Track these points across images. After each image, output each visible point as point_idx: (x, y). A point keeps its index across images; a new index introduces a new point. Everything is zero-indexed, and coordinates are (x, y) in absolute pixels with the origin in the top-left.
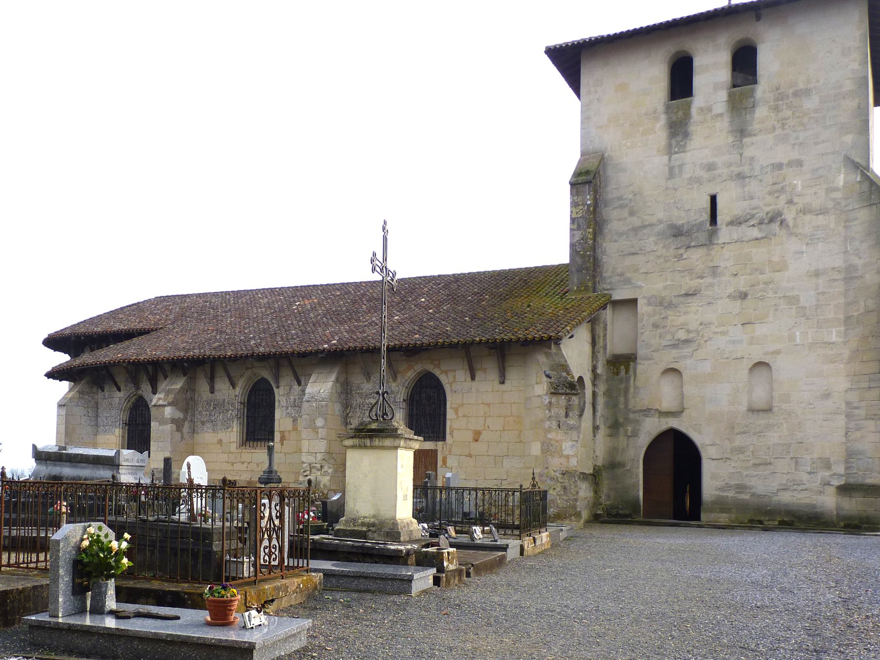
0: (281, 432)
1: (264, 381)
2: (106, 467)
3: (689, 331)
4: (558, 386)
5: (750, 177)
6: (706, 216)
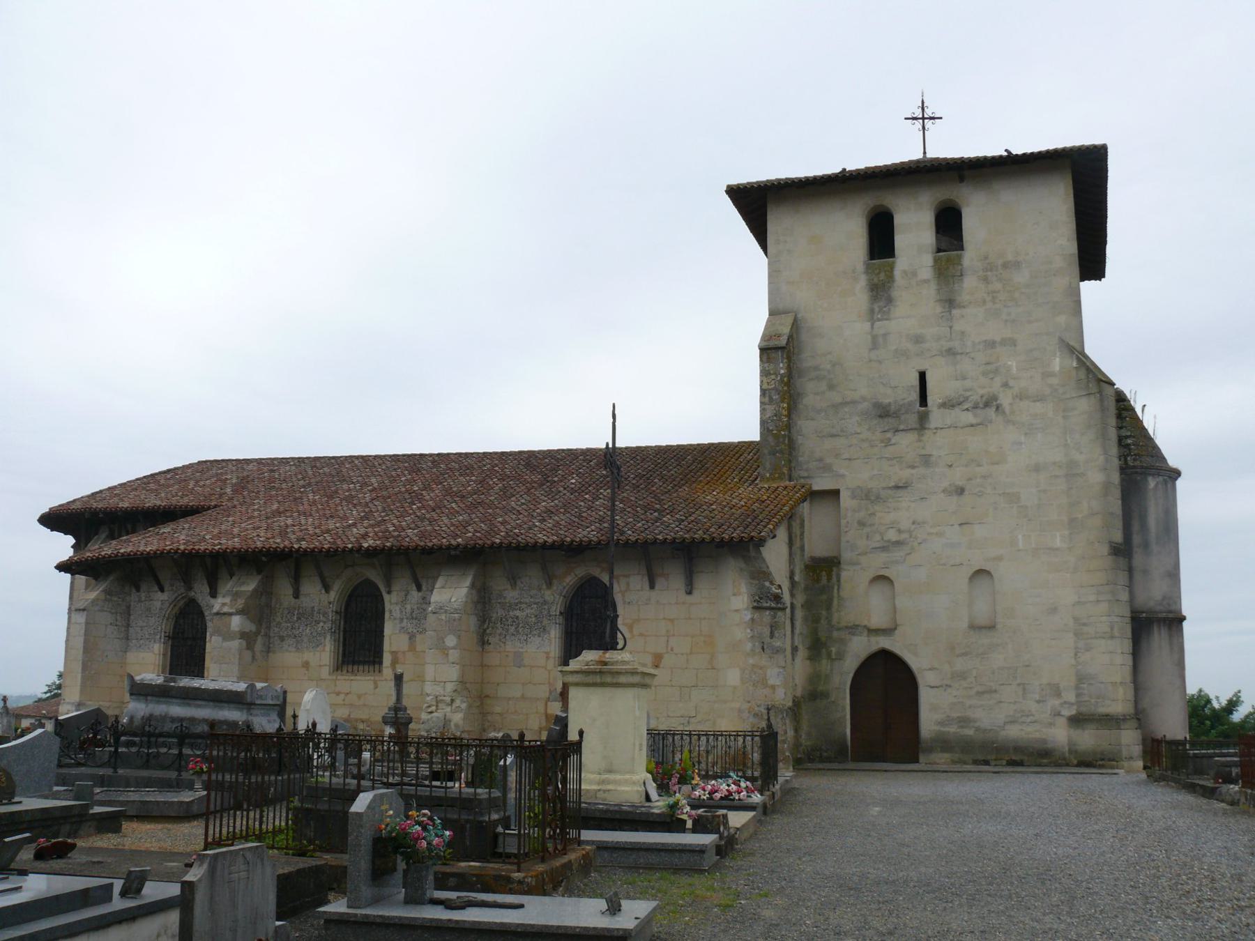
1: (369, 583)
2: (232, 706)
3: (900, 531)
4: (761, 598)
5: (962, 354)
6: (915, 396)
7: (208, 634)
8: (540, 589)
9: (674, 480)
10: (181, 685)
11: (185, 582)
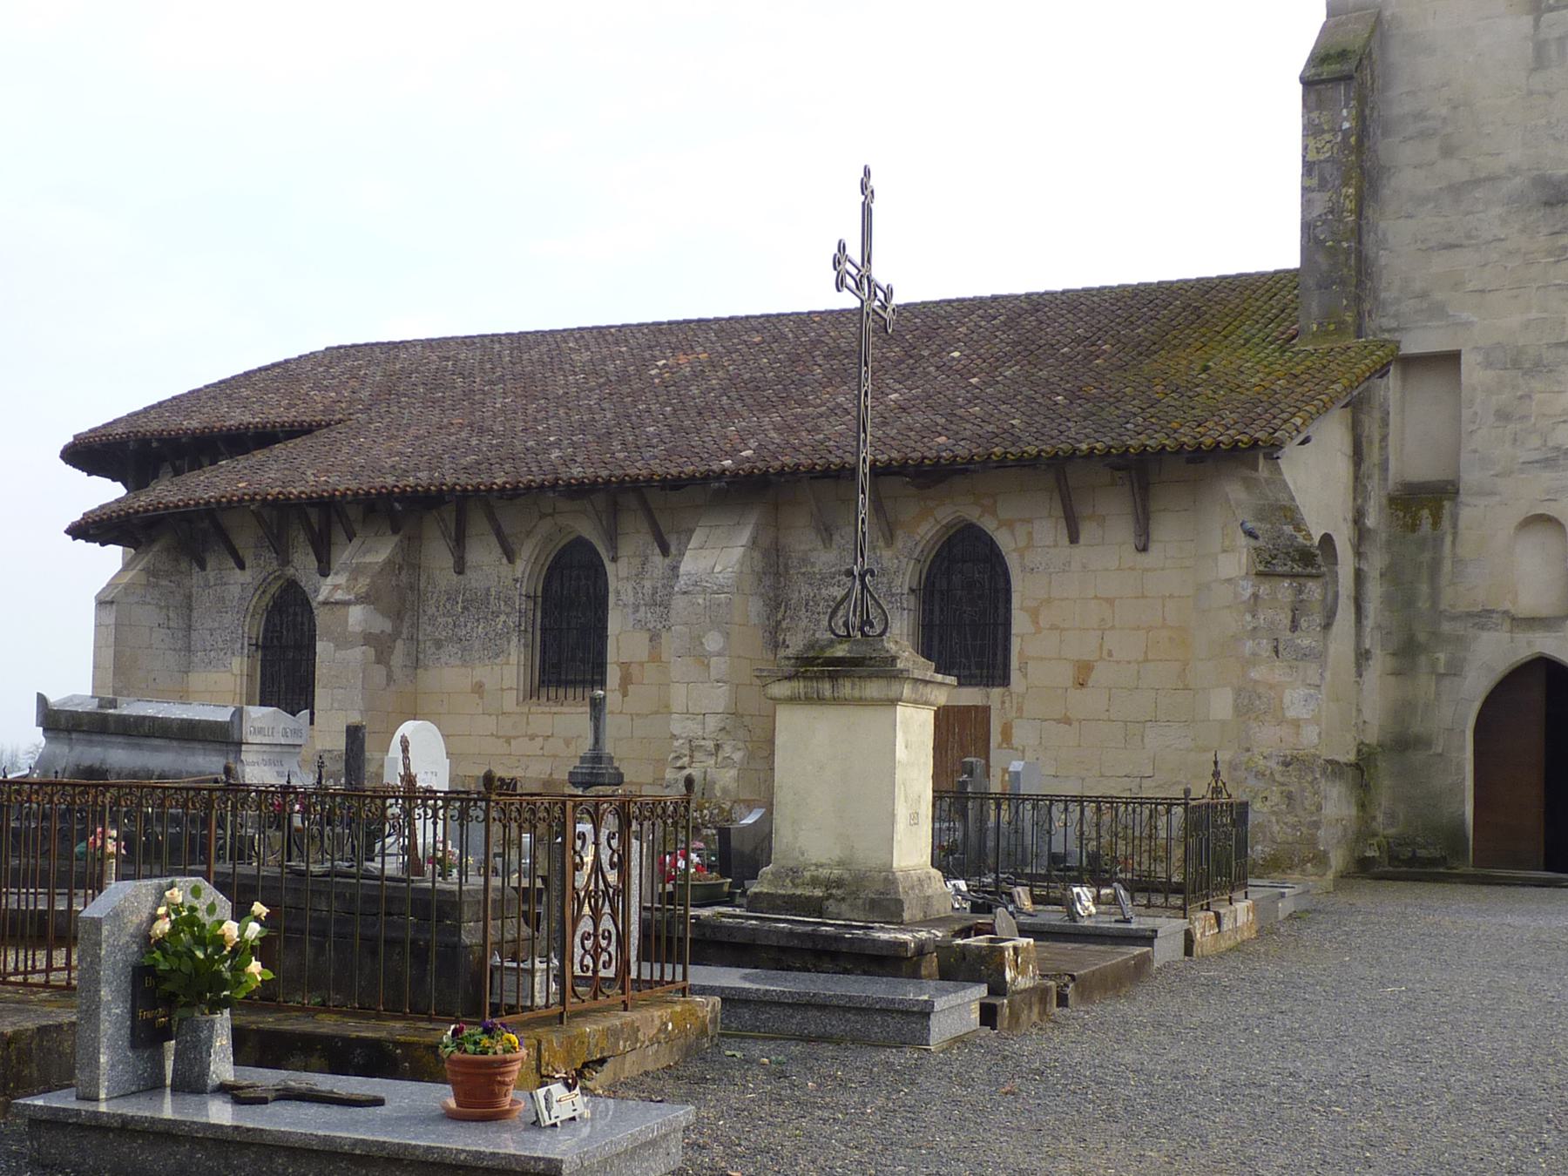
1: (581, 544)
2: (210, 747)
9: (1139, 345)
10: (125, 713)
11: (276, 552)
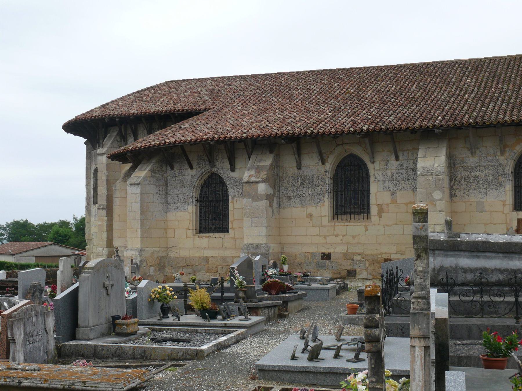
0: (378, 205)
7: (230, 197)
8: (495, 156)
